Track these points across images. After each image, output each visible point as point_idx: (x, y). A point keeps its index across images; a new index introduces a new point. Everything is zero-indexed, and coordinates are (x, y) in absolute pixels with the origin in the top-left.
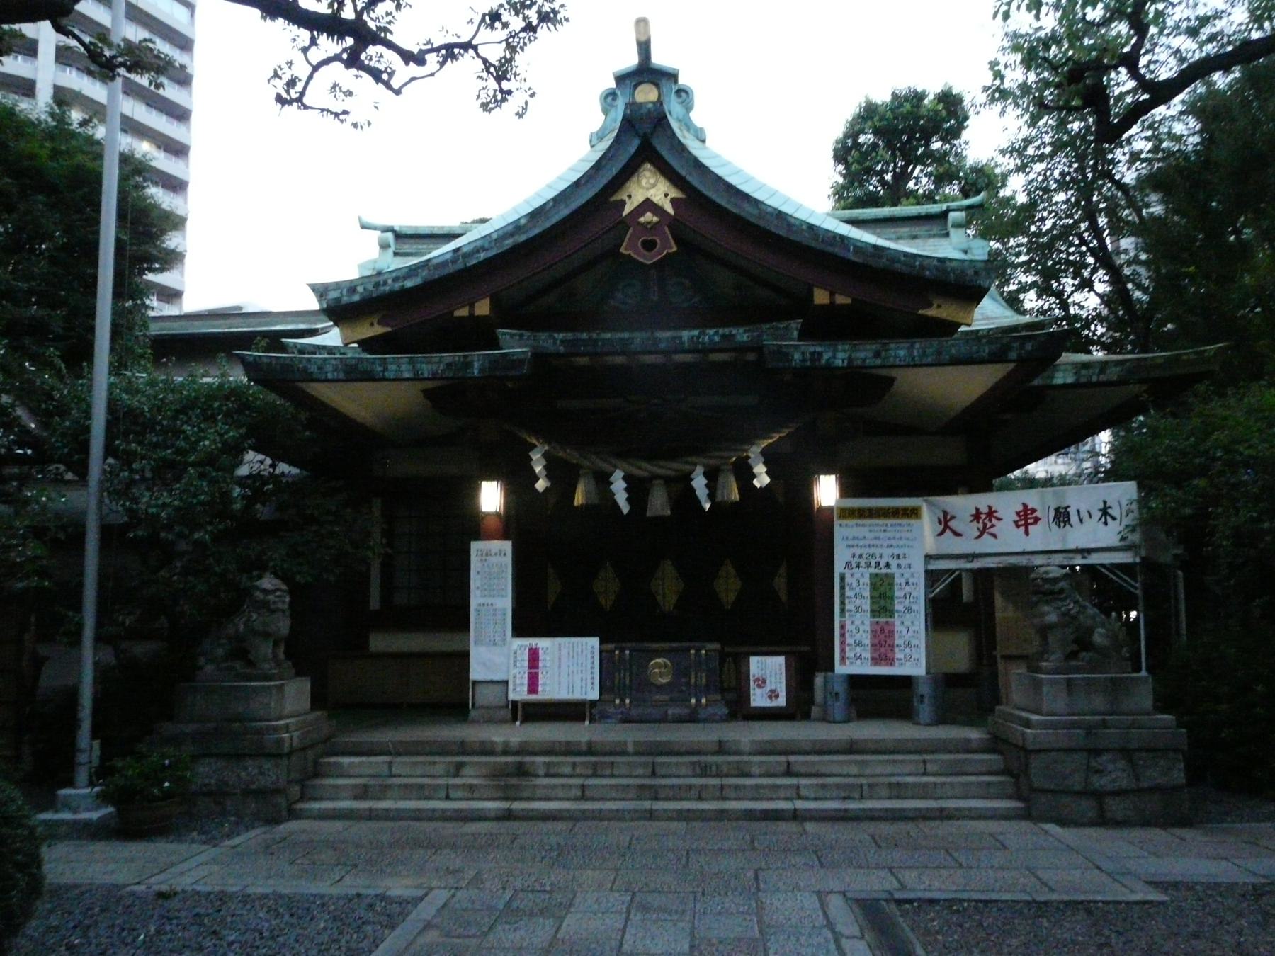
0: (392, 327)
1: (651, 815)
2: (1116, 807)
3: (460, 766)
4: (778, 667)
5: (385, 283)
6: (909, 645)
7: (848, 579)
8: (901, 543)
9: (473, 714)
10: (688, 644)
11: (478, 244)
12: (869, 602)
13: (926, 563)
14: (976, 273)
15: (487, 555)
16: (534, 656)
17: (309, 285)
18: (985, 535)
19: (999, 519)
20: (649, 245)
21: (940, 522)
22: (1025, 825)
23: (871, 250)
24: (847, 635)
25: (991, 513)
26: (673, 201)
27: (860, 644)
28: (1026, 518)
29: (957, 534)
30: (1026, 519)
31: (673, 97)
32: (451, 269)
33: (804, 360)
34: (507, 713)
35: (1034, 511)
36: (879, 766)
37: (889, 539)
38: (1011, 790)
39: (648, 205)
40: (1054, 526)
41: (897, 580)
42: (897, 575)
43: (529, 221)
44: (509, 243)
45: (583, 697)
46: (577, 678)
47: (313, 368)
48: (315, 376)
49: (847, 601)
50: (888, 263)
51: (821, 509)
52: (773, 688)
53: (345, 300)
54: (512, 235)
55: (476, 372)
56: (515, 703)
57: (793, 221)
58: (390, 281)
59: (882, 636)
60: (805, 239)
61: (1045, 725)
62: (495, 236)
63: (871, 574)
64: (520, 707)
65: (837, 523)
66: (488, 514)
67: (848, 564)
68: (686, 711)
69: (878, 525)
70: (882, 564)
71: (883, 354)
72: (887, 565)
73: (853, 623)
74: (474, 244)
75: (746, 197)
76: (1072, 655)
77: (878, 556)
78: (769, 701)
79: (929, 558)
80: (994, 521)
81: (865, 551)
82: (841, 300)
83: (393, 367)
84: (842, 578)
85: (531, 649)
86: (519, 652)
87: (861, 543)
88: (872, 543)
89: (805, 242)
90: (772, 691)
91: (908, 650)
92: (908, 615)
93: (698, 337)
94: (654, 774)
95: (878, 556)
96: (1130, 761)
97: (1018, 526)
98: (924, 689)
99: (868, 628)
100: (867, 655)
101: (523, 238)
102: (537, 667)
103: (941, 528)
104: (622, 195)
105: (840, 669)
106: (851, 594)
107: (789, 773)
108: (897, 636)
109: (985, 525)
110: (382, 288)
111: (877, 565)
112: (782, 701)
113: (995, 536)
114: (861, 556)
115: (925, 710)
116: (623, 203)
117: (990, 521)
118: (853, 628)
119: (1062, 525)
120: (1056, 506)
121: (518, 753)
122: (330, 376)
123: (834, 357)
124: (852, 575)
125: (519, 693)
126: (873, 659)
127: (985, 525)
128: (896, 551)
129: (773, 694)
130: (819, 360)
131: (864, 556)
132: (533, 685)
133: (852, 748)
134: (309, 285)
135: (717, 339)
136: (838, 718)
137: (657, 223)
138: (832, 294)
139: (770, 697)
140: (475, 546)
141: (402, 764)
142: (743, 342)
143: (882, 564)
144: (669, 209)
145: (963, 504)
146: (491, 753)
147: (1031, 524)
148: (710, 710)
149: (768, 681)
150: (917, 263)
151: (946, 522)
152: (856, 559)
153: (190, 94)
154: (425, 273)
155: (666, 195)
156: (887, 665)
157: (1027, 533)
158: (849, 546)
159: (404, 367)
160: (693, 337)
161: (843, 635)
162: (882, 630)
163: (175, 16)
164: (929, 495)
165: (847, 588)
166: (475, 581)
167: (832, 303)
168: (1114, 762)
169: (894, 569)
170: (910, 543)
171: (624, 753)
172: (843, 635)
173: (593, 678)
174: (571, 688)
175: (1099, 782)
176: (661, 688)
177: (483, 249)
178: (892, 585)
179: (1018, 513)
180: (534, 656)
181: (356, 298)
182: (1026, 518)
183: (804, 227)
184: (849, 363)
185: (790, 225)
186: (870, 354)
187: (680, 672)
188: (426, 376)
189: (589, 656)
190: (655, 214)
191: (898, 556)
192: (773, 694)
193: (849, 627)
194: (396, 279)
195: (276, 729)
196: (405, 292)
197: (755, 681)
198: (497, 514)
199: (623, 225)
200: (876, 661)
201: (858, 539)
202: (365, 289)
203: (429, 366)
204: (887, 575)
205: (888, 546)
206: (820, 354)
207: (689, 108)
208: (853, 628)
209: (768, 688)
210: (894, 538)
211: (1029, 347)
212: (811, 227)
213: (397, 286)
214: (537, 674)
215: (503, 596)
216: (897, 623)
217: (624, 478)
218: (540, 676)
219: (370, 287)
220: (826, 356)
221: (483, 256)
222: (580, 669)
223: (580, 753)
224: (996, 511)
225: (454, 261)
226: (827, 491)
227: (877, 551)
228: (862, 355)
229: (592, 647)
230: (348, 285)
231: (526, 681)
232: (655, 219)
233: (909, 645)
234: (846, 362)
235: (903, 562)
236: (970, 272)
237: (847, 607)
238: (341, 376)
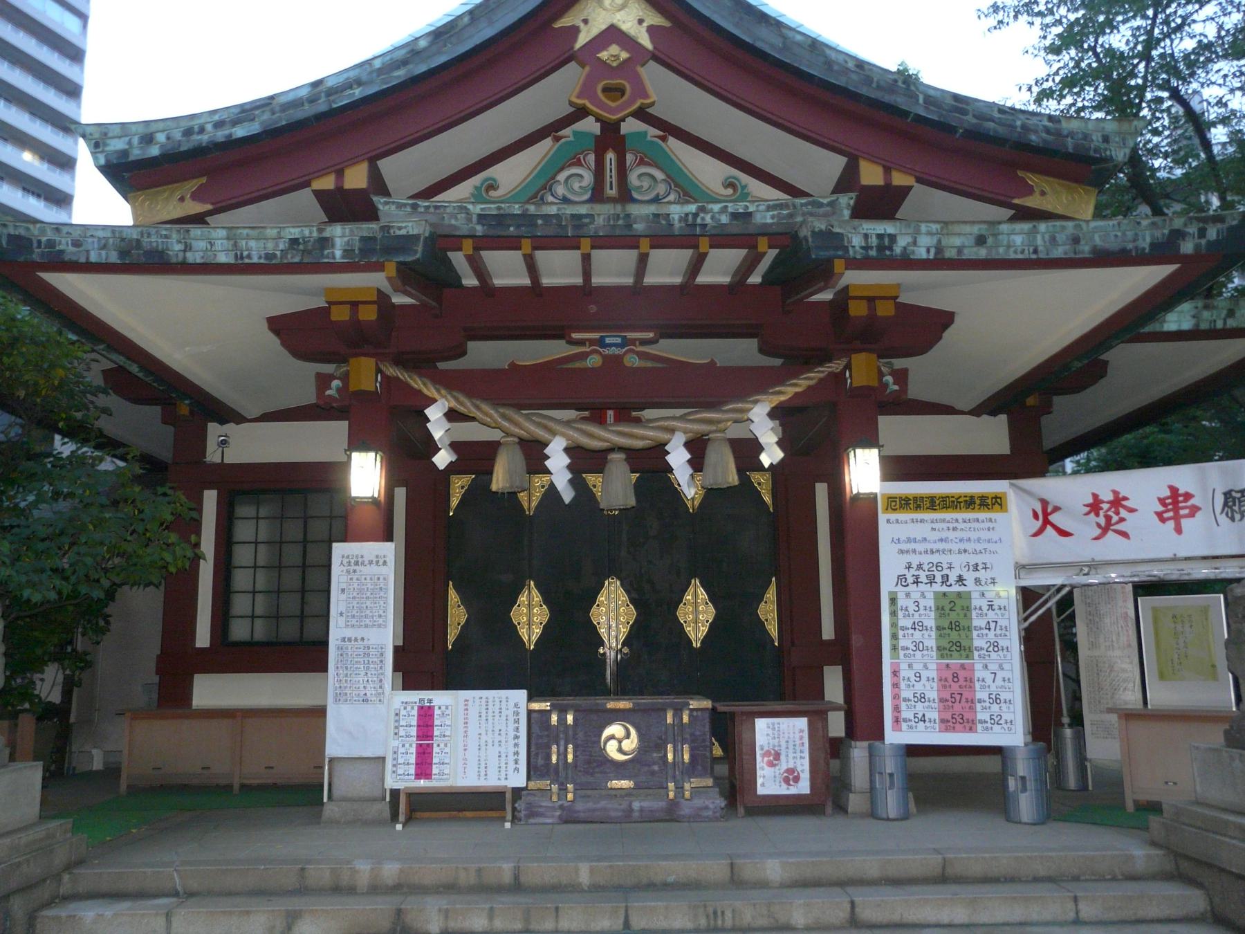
0: (212, 204)
4: (797, 736)
5: (202, 130)
6: (997, 700)
7: (901, 602)
8: (979, 547)
9: (330, 810)
10: (659, 700)
11: (352, 74)
12: (933, 634)
13: (1017, 577)
14: (1106, 139)
15: (357, 563)
16: (426, 717)
18: (1110, 534)
19: (1132, 510)
21: (1036, 516)
23: (950, 101)
24: (903, 685)
25: (1118, 502)
26: (652, 30)
27: (922, 698)
29: (1063, 533)
30: (1176, 509)
32: (308, 111)
33: (866, 248)
34: (384, 809)
35: (1188, 496)
37: (961, 540)
39: (613, 34)
40: (1223, 519)
41: (976, 602)
42: (975, 595)
43: (432, 44)
44: (401, 74)
45: (503, 783)
46: (493, 752)
47: (65, 245)
48: (67, 258)
49: (901, 633)
50: (974, 121)
51: (857, 498)
52: (791, 766)
53: (136, 154)
54: (404, 63)
55: (338, 253)
56: (395, 793)
57: (833, 55)
58: (209, 127)
59: (955, 687)
60: (851, 82)
62: (377, 64)
63: (935, 593)
64: (403, 800)
65: (882, 518)
66: (362, 502)
67: (901, 579)
68: (662, 804)
69: (943, 521)
70: (952, 579)
71: (990, 241)
72: (960, 579)
73: (910, 666)
74: (345, 76)
77: (945, 566)
78: (784, 786)
79: (1021, 568)
80: (1123, 513)
81: (926, 559)
83: (202, 245)
84: (893, 601)
85: (421, 708)
86: (403, 712)
87: (920, 547)
88: (935, 547)
90: (790, 771)
91: (995, 708)
92: (993, 655)
93: (696, 215)
95: (945, 566)
97: (1163, 520)
99: (934, 674)
100: (933, 715)
101: (422, 68)
102: (430, 737)
103: (1039, 523)
105: (894, 737)
106: (907, 623)
108: (978, 685)
109: (1108, 518)
110: (196, 137)
111: (945, 579)
112: (803, 787)
113: (1125, 534)
114: (920, 567)
116: (575, 31)
117: (1117, 513)
118: (911, 674)
119: (1237, 517)
120: (1225, 490)
122: (93, 258)
123: (915, 243)
124: (908, 595)
125: (401, 777)
126: (942, 721)
127: (1108, 518)
128: (973, 559)
129: (791, 776)
130: (890, 249)
131: (926, 567)
132: (424, 766)
135: (724, 219)
136: (892, 814)
137: (626, 61)
138: (887, 170)
139: (787, 781)
140: (339, 549)
142: (766, 225)
143: (952, 579)
144: (645, 41)
146: (351, 891)
147: (1186, 516)
148: (698, 802)
149: (783, 757)
150: (1019, 123)
151: (1046, 514)
152: (913, 572)
153: (79, 106)
154: (266, 116)
155: (641, 21)
156: (964, 730)
157: (1179, 530)
158: (901, 552)
159: (219, 245)
160: (687, 215)
161: (896, 685)
162: (955, 676)
163: (65, 23)
164: (1016, 477)
165: (900, 614)
166: (338, 603)
169: (970, 586)
170: (990, 546)
172: (896, 685)
173: (517, 753)
174: (484, 770)
176: (620, 769)
177: (359, 82)
178: (967, 609)
179: (1162, 501)
180: (426, 717)
181: (154, 151)
183: (851, 65)
184: (936, 254)
185: (829, 63)
186: (970, 241)
187: (651, 744)
188: (255, 260)
189: (511, 718)
190: (624, 48)
191: (976, 567)
192: (791, 776)
193: (905, 672)
194: (219, 125)
196: (231, 144)
197: (764, 755)
198: (374, 501)
200: (948, 724)
201: (915, 540)
202: (168, 138)
203: (261, 244)
204: (959, 594)
205: (960, 552)
206: (893, 238)
208: (911, 674)
209: (784, 765)
210: (969, 540)
213: (220, 135)
214: (430, 746)
215: (379, 626)
216: (978, 666)
217: (567, 450)
218: (436, 749)
219: (177, 135)
220: (902, 242)
221: (358, 93)
222: (498, 738)
224: (1126, 499)
225: (312, 100)
227: (944, 559)
228: (957, 241)
229: (516, 705)
230: (141, 130)
231: (413, 759)
232: (624, 55)
233: (997, 700)
234: (933, 251)
235: (982, 574)
236: (1097, 138)
237: (903, 643)
238: (114, 258)
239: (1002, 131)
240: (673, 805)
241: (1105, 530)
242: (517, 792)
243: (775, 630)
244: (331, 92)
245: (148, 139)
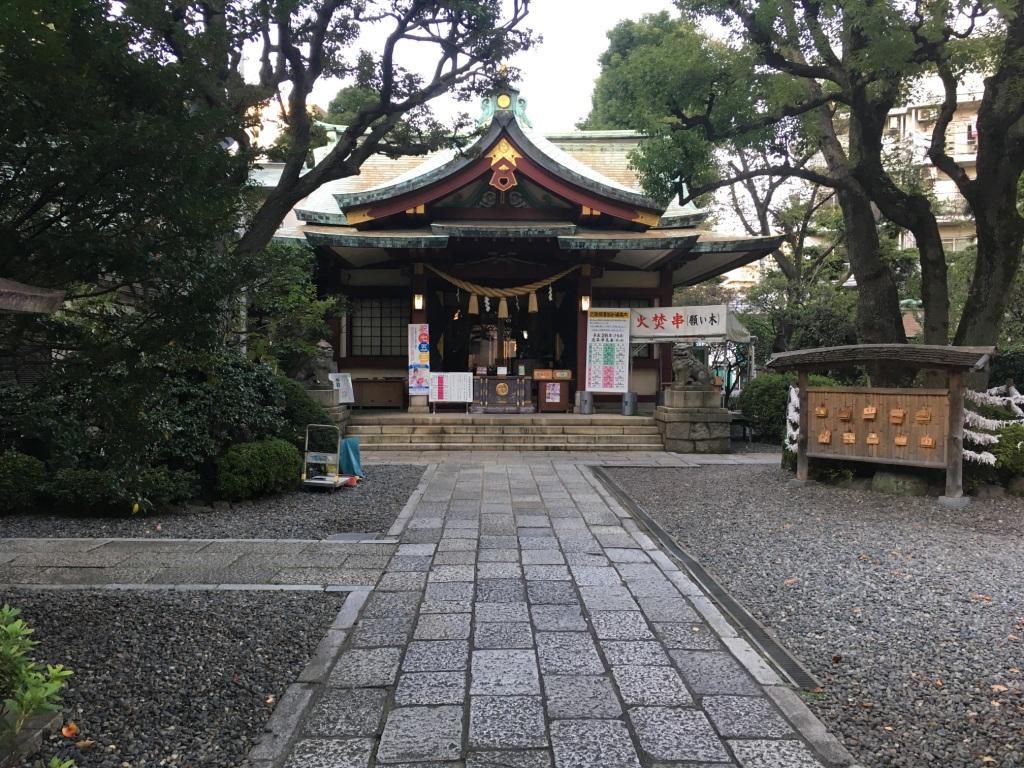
1: (504, 449)
2: (701, 446)
3: (414, 429)
16: (441, 380)
17: (334, 195)
20: (504, 181)
22: (663, 453)
25: (662, 317)
26: (516, 159)
28: (678, 320)
31: (517, 103)
32: (406, 190)
36: (602, 431)
38: (660, 440)
39: (504, 161)
44: (436, 178)
53: (352, 204)
54: (437, 174)
56: (432, 403)
61: (674, 412)
75: (552, 161)
76: (689, 383)
82: (596, 213)
89: (580, 185)
94: (503, 433)
96: (708, 427)
98: (627, 399)
104: (490, 155)
107: (563, 433)
115: (628, 409)
116: (491, 159)
121: (439, 424)
125: (434, 398)
132: (441, 394)
133: (592, 424)
134: (334, 195)
138: (592, 209)
141: (387, 429)
145: (649, 313)
146: (428, 424)
154: (393, 192)
157: (678, 327)
167: (591, 215)
168: (701, 427)
171: (489, 425)
175: (695, 436)
177: (422, 181)
180: (441, 380)
181: (358, 203)
182: (678, 320)
185: (573, 176)
193: (593, 369)
194: (378, 194)
195: (334, 411)
199: (490, 172)
200: (605, 385)
207: (524, 108)
211: (679, 243)
212: (583, 177)
213: (379, 198)
221: (422, 185)
223: (469, 424)
225: (408, 186)
226: (586, 304)
239: (627, 200)
240: (519, 409)
241: (657, 326)
242: (470, 404)
243: (90, 543)
244: (414, 184)
245: (356, 199)
